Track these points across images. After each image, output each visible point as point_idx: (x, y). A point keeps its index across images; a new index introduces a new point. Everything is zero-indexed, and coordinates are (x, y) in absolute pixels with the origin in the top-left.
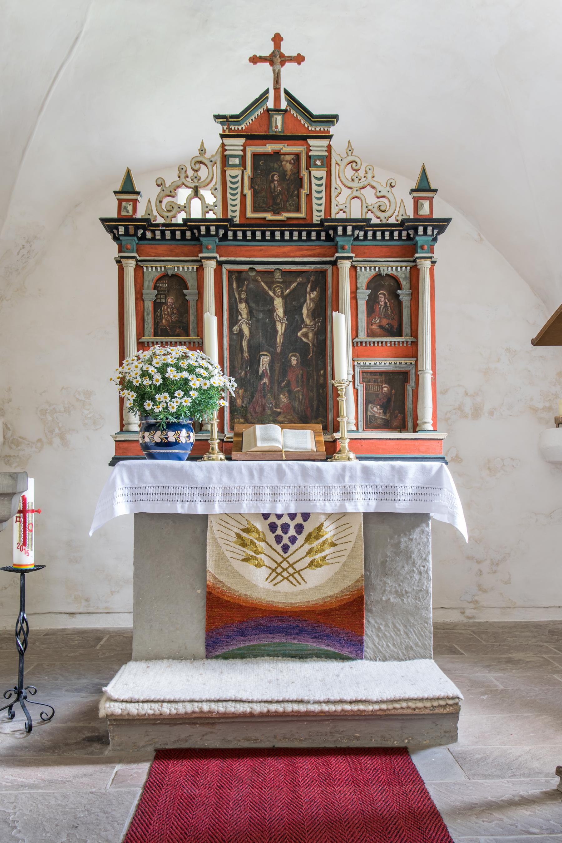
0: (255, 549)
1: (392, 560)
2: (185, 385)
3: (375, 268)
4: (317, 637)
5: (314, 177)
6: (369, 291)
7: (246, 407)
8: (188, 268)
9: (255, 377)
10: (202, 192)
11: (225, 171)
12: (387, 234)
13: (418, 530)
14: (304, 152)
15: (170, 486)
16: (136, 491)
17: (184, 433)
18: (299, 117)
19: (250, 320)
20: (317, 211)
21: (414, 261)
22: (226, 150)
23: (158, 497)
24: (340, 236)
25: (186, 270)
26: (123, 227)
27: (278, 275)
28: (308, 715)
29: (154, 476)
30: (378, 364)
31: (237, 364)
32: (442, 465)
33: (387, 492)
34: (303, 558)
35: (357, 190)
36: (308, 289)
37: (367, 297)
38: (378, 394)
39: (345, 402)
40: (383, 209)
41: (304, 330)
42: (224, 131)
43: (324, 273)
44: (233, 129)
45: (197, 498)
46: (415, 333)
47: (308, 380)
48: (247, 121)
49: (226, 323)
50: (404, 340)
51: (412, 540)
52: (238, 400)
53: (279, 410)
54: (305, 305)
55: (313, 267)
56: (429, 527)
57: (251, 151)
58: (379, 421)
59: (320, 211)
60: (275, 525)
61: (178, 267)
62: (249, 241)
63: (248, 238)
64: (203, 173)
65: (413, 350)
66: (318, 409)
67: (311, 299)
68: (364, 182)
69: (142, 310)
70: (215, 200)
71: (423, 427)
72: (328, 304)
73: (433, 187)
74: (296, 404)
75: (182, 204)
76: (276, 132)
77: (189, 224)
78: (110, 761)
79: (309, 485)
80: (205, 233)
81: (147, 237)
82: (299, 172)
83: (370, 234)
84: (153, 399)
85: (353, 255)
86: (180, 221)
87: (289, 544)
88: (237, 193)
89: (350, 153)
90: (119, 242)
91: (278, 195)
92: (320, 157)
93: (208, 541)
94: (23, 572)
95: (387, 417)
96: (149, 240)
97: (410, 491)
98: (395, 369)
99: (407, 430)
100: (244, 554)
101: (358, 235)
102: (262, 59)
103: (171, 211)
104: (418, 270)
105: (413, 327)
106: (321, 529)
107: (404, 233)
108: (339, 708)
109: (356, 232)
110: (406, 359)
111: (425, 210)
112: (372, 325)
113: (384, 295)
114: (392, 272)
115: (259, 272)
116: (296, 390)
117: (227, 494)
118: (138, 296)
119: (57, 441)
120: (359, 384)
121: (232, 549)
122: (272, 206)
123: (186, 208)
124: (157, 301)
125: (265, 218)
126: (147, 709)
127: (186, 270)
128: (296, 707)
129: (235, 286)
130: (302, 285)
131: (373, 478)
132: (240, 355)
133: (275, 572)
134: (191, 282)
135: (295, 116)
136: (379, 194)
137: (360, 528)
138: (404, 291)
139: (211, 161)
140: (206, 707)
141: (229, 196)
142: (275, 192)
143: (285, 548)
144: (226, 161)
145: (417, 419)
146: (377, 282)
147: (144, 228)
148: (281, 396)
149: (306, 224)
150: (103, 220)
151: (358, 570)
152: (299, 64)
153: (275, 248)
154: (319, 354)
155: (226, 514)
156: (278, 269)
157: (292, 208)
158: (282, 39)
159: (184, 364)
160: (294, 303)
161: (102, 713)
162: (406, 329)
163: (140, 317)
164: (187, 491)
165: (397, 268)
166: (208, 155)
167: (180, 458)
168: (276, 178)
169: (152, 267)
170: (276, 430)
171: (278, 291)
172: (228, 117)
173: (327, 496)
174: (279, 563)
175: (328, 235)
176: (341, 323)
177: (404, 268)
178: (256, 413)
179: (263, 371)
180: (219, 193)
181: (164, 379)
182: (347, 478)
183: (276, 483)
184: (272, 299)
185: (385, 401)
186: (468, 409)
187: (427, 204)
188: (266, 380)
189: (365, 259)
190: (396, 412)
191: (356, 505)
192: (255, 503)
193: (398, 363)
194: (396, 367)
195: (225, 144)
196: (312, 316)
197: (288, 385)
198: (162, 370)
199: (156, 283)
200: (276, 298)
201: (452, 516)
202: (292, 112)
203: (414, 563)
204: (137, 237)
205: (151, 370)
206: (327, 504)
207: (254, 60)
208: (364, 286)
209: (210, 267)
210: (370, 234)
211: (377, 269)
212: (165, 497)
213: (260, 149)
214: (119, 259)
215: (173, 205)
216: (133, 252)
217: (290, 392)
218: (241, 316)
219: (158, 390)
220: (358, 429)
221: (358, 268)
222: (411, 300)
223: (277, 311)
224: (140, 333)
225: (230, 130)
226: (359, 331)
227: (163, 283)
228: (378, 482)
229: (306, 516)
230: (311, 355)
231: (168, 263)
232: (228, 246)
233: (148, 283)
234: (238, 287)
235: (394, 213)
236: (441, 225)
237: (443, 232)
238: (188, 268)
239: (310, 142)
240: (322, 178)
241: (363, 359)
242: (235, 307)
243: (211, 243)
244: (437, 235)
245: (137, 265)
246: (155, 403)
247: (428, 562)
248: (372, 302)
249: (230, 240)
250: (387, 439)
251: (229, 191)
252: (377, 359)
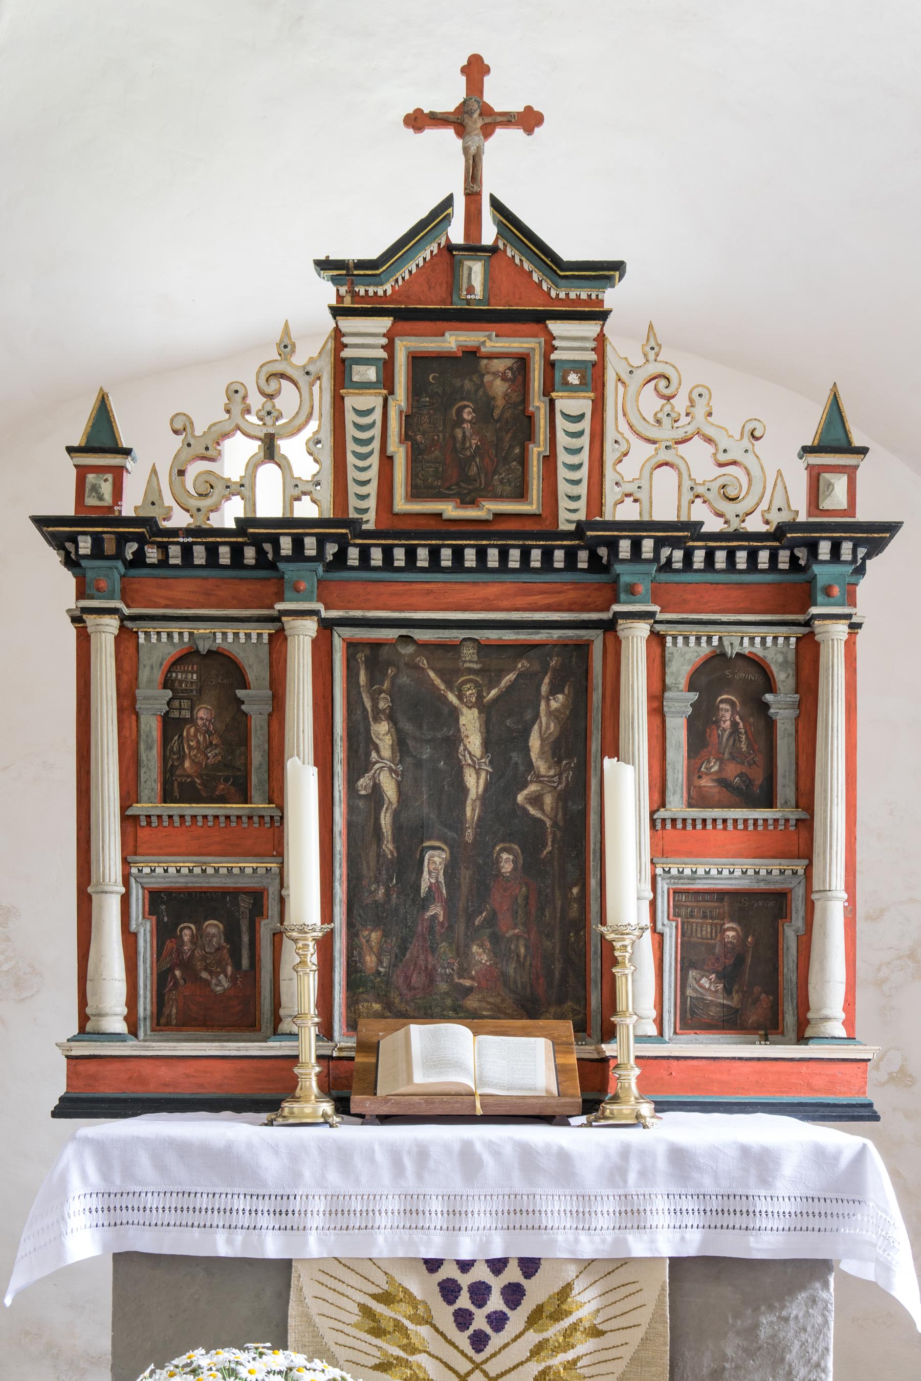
0: (405, 1341)
1: (737, 1367)
3: (709, 639)
5: (563, 414)
6: (694, 696)
7: (387, 975)
8: (248, 636)
9: (409, 902)
10: (285, 446)
11: (343, 398)
12: (741, 557)
13: (802, 1296)
14: (537, 352)
15: (199, 1190)
16: (117, 1202)
18: (527, 266)
19: (401, 762)
20: (569, 497)
21: (807, 624)
22: (346, 346)
23: (170, 1217)
24: (624, 561)
25: (243, 640)
26: (89, 539)
27: (469, 653)
29: (160, 1166)
30: (714, 872)
31: (368, 870)
32: (864, 1146)
33: (731, 1210)
34: (522, 1363)
35: (671, 450)
36: (544, 689)
37: (690, 710)
38: (714, 946)
39: (630, 977)
40: (732, 493)
41: (533, 788)
42: (340, 298)
43: (583, 648)
44: (362, 293)
45: (264, 1221)
46: (806, 799)
47: (542, 910)
48: (398, 275)
49: (340, 770)
50: (778, 815)
51: (786, 1320)
52: (368, 958)
53: (468, 983)
54: (536, 727)
55: (556, 634)
56: (828, 1289)
57: (407, 348)
58: (713, 1011)
59: (577, 498)
61: (224, 635)
62: (399, 570)
63: (396, 564)
64: (288, 400)
65: (801, 840)
66: (562, 983)
67: (550, 713)
69: (134, 736)
70: (316, 468)
71: (823, 1029)
72: (593, 727)
73: (858, 440)
74: (511, 969)
75: (236, 479)
76: (468, 302)
77: (251, 530)
79: (539, 1191)
80: (290, 553)
81: (148, 561)
82: (524, 399)
83: (699, 557)
85: (657, 608)
86: (231, 524)
87: (488, 1330)
88: (372, 452)
89: (651, 355)
90: (77, 570)
91: (473, 457)
93: (291, 1322)
95: (734, 1001)
96: (152, 566)
97: (787, 1206)
98: (755, 886)
99: (783, 1033)
100: (378, 1354)
101: (669, 560)
102: (437, 120)
103: (206, 495)
104: (817, 645)
105: (801, 784)
106: (568, 1296)
107: (784, 556)
109: (665, 552)
110: (783, 861)
111: (837, 496)
112: (700, 777)
113: (732, 704)
114: (753, 650)
115: (424, 647)
116: (510, 933)
117: (338, 1211)
118: (126, 703)
120: (666, 921)
121: (350, 1341)
122: (457, 484)
123: (245, 488)
124: (172, 715)
125: (440, 515)
127: (243, 640)
129: (363, 678)
130: (529, 680)
131: (696, 1175)
132: (374, 846)
135: (517, 261)
136: (723, 458)
137: (661, 1295)
138: (781, 697)
139: (308, 373)
141: (351, 459)
142: (464, 448)
143: (479, 1341)
144: (344, 372)
145: (808, 1009)
146: (714, 673)
147: (141, 540)
148: (475, 949)
149: (540, 532)
150: (41, 522)
152: (529, 131)
153: (463, 586)
154: (571, 849)
155: (336, 1258)
156: (470, 639)
157: (508, 488)
158: (487, 70)
160: (508, 722)
162: (785, 788)
163: (129, 753)
164: (240, 1204)
165: (763, 640)
166: (300, 359)
168: (467, 415)
169: (159, 633)
170: (457, 1036)
171: (470, 692)
172: (351, 265)
173: (582, 1217)
174: (462, 1373)
175: (594, 558)
176: (625, 788)
177: (781, 640)
178: (410, 988)
179: (430, 888)
180: (326, 450)
182: (632, 1177)
183: (457, 1185)
184: (454, 713)
185: (730, 962)
187: (840, 484)
188: (436, 910)
189: (685, 616)
190: (757, 989)
191: (653, 1241)
192: (405, 1234)
193: (763, 872)
194: (758, 881)
195: (343, 330)
196: (554, 755)
197: (492, 921)
199: (169, 671)
200: (465, 710)
201: (886, 1268)
202: (509, 254)
203: (790, 1373)
204: (124, 560)
206: (583, 1237)
207: (418, 121)
208: (683, 682)
209: (303, 635)
210: (699, 557)
211: (715, 642)
212: (188, 1218)
213: (429, 345)
214: (78, 613)
215: (212, 480)
216: (112, 598)
217: (496, 939)
218: (378, 752)
220: (661, 1033)
221: (669, 640)
222: (797, 719)
223: (466, 741)
225: (354, 295)
226: (669, 793)
227: (186, 672)
228: (708, 1185)
229: (530, 1266)
230: (549, 848)
231: (199, 624)
232: (348, 581)
233: (150, 672)
234: (372, 681)
235: (758, 504)
236: (877, 536)
237: (881, 551)
238: (248, 636)
239: (554, 326)
240: (582, 416)
241: (678, 860)
242: (362, 730)
243: (306, 577)
244: (864, 559)
245: (122, 627)
247: (824, 1371)
248: (701, 724)
249: (352, 568)
250: (734, 1058)
251: (351, 446)
252: (711, 860)
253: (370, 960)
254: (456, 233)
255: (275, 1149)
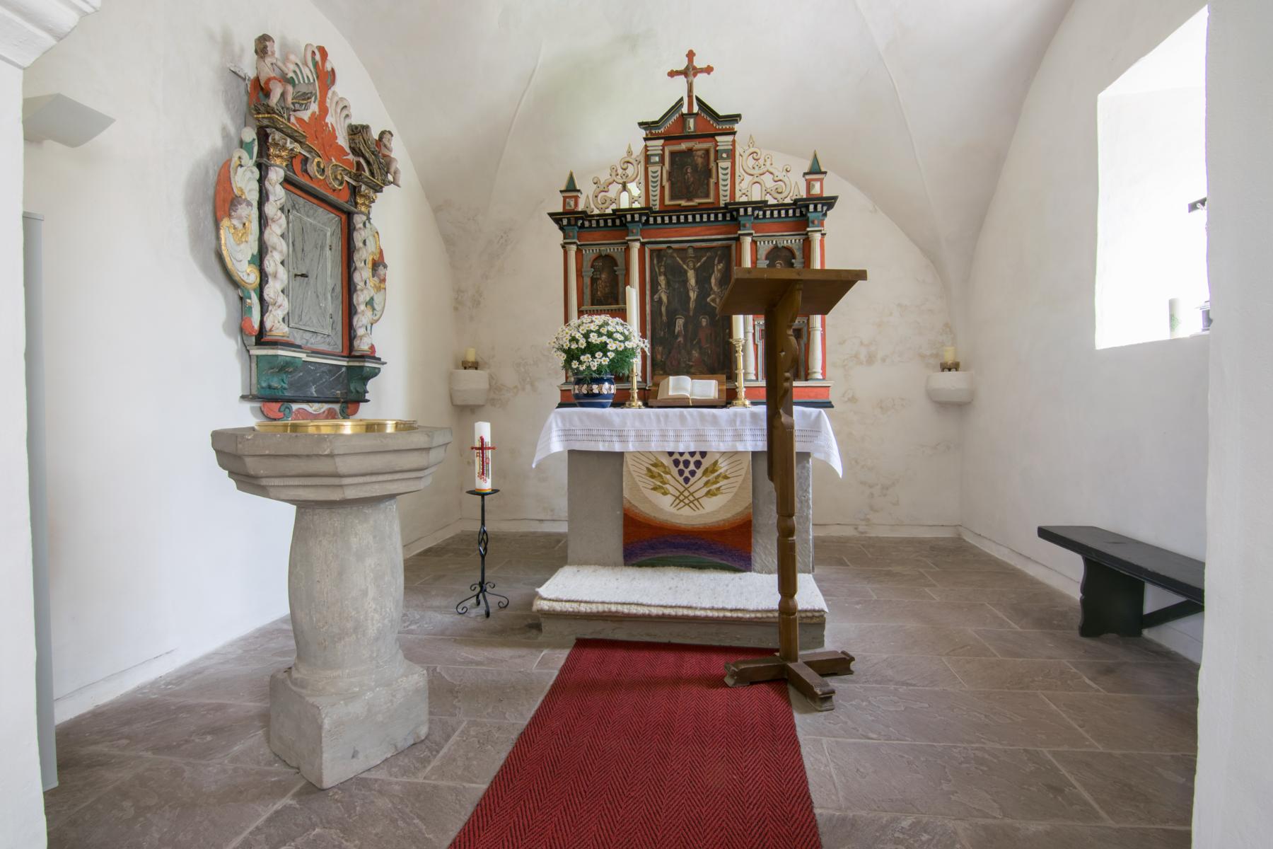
2: (603, 348)
4: (713, 553)
10: (629, 186)
12: (783, 212)
17: (607, 385)
27: (690, 251)
28: (695, 618)
29: (581, 420)
43: (729, 247)
45: (615, 439)
49: (648, 293)
60: (678, 460)
64: (631, 170)
68: (763, 169)
73: (823, 169)
78: (540, 646)
83: (768, 213)
84: (578, 359)
92: (726, 151)
94: (483, 495)
108: (721, 614)
111: (816, 190)
119: (528, 387)
126: (568, 607)
128: (686, 612)
130: (711, 259)
133: (679, 499)
134: (620, 261)
140: (613, 608)
143: (687, 480)
149: (713, 208)
150: (551, 215)
151: (748, 499)
159: (604, 331)
161: (535, 608)
166: (634, 156)
167: (603, 406)
171: (691, 264)
173: (721, 437)
175: (732, 216)
180: (643, 186)
181: (588, 343)
184: (686, 272)
186: (862, 357)
188: (680, 339)
197: (699, 342)
198: (586, 336)
201: (828, 455)
205: (578, 336)
210: (768, 213)
217: (701, 348)
219: (584, 352)
224: (580, 304)
229: (703, 454)
236: (830, 202)
239: (718, 138)
246: (581, 363)
253: (659, 357)
254: (685, 110)
255: (618, 415)
